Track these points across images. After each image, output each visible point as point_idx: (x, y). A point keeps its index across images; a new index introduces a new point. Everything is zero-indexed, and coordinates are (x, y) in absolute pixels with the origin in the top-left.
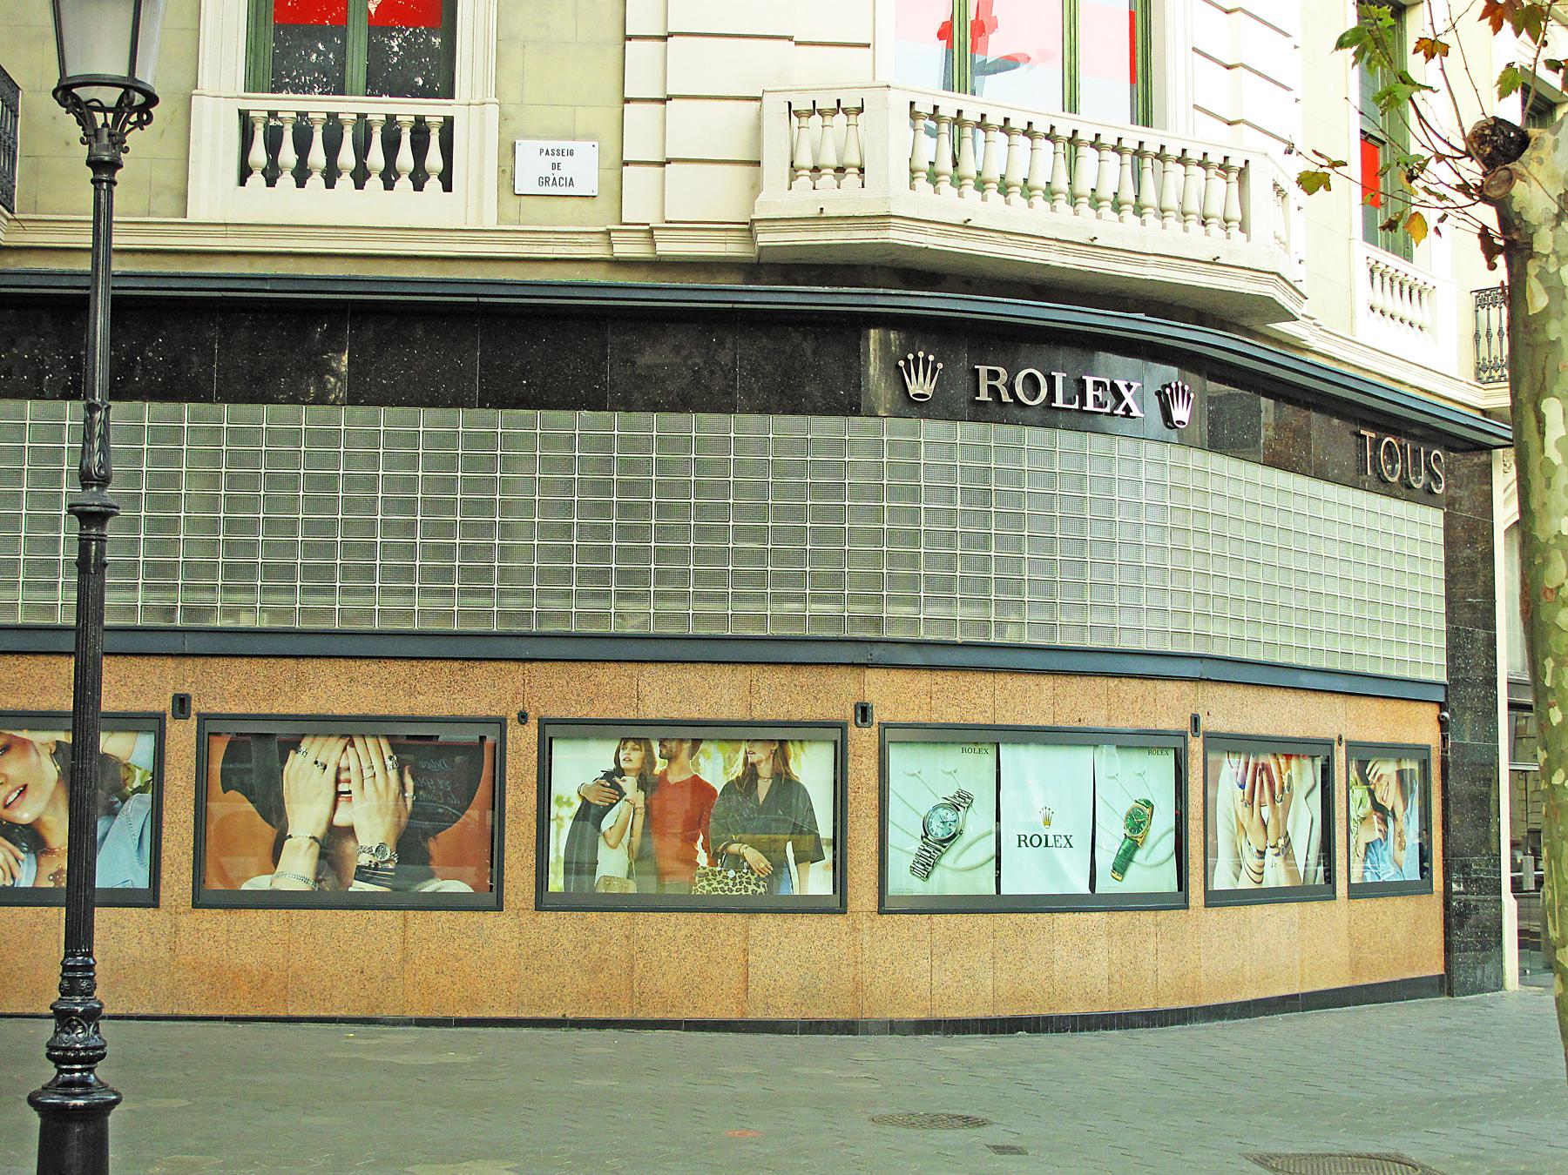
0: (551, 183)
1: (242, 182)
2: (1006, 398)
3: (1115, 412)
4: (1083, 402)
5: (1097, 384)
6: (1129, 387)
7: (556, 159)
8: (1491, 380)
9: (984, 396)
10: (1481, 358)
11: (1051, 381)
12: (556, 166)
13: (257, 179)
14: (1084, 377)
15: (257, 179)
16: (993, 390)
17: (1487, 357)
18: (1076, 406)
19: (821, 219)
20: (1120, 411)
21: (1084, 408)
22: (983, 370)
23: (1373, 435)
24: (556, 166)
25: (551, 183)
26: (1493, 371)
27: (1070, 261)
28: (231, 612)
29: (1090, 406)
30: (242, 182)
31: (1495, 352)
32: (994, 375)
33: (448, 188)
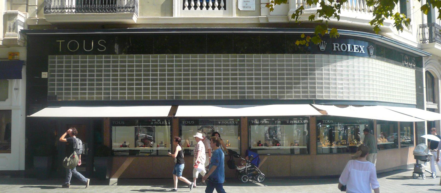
0: (246, 7)
1: (183, 9)
2: (339, 50)
3: (360, 52)
4: (354, 50)
5: (356, 47)
6: (362, 47)
7: (247, 3)
8: (58, 12)
9: (335, 49)
10: (55, 6)
11: (347, 46)
12: (246, 4)
13: (187, 8)
14: (354, 45)
15: (187, 8)
16: (337, 48)
17: (68, 5)
18: (352, 51)
19: (355, 19)
20: (360, 52)
21: (354, 52)
22: (335, 44)
23: (363, 52)
24: (246, 4)
25: (246, 7)
26: (55, 10)
27: (349, 22)
28: (288, 97)
29: (355, 51)
30: (183, 9)
31: (56, 4)
32: (337, 45)
33: (225, 9)
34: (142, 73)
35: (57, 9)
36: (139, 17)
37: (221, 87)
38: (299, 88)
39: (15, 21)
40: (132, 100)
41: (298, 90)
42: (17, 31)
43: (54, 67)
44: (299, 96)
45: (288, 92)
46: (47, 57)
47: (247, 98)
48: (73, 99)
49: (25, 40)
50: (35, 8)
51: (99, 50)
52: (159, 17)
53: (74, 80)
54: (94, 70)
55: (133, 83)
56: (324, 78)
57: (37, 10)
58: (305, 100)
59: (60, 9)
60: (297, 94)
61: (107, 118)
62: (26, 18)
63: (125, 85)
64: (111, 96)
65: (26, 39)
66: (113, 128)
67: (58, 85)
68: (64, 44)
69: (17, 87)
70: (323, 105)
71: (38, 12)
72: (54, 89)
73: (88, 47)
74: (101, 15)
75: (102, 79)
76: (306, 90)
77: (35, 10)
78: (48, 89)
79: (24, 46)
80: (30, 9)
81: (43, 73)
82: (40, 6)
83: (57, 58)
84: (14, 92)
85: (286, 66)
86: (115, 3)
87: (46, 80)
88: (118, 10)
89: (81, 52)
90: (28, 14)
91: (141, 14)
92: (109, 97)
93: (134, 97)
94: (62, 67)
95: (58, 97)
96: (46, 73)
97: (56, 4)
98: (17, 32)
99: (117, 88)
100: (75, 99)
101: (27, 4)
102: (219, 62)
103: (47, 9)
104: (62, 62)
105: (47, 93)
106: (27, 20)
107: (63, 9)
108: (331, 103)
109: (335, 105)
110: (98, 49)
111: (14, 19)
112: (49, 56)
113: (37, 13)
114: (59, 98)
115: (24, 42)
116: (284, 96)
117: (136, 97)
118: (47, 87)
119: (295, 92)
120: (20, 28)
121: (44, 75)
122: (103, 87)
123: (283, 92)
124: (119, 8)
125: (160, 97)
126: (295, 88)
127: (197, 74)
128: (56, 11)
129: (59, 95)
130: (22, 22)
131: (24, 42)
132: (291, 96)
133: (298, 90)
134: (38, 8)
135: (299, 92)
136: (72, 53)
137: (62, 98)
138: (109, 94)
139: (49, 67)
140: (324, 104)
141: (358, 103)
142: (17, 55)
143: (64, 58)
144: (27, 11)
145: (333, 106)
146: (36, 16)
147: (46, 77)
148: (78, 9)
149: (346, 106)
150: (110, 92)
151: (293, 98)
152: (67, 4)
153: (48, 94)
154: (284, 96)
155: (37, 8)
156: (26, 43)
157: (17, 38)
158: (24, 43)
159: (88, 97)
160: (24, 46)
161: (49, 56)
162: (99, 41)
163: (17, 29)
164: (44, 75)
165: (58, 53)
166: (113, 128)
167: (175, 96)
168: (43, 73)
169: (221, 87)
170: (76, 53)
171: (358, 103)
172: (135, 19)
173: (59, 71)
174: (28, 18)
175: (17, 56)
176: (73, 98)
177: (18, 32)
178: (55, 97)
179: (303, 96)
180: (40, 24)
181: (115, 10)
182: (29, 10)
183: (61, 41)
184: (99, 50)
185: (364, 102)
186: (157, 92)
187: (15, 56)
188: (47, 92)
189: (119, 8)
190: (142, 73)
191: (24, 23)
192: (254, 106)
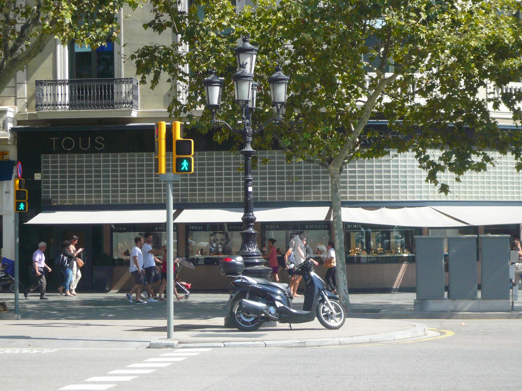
28: (306, 198)
31: (49, 100)
34: (127, 158)
35: (49, 105)
36: (140, 110)
37: (231, 188)
38: (319, 188)
39: (4, 118)
40: (125, 203)
41: (318, 190)
42: (7, 129)
43: (48, 167)
44: (319, 198)
45: (306, 193)
46: (40, 157)
47: (260, 200)
48: (69, 203)
49: (15, 137)
50: (24, 102)
51: (97, 148)
52: (162, 110)
53: (70, 182)
54: (92, 170)
55: (135, 185)
56: (401, 170)
57: (27, 103)
58: (325, 202)
59: (53, 105)
60: (316, 196)
61: (107, 224)
62: (15, 112)
63: (126, 187)
64: (110, 199)
65: (16, 136)
66: (115, 234)
67: (53, 187)
68: (58, 143)
69: (7, 191)
70: (347, 207)
71: (28, 105)
72: (48, 192)
73: (85, 145)
74: (97, 112)
75: (100, 180)
76: (345, 190)
77: (24, 103)
78: (42, 193)
79: (14, 144)
80: (19, 102)
81: (36, 174)
82: (30, 99)
83: (50, 158)
84: (5, 195)
85: (258, 177)
86: (113, 98)
87: (39, 182)
88: (115, 106)
89: (77, 151)
90: (17, 107)
91: (143, 106)
92: (109, 200)
93: (223, 198)
94: (56, 167)
95: (53, 201)
96: (40, 174)
97: (49, 100)
98: (6, 131)
99: (118, 190)
100: (72, 203)
101: (15, 97)
102: (229, 160)
103: (38, 105)
104: (56, 162)
105: (41, 197)
106: (16, 116)
107: (57, 105)
108: (357, 205)
109: (362, 207)
110: (96, 147)
111: (4, 116)
112: (42, 156)
113: (27, 107)
114: (54, 202)
115: (14, 139)
116: (301, 198)
117: (207, 199)
118: (40, 190)
119: (315, 193)
120: (10, 126)
121: (38, 176)
122: (102, 189)
123: (301, 193)
124: (116, 104)
125: (287, 198)
126: (314, 188)
127: (205, 168)
128: (49, 107)
129: (53, 198)
130: (11, 118)
131: (14, 139)
132: (310, 198)
133: (318, 190)
134: (27, 101)
135: (318, 193)
136: (67, 152)
137: (57, 202)
138: (117, 196)
139: (42, 167)
140: (347, 206)
141: (395, 205)
142: (6, 154)
143: (59, 157)
144: (16, 105)
145: (360, 209)
146: (26, 110)
147: (39, 178)
148: (72, 105)
149: (379, 207)
150: (109, 195)
151: (312, 200)
152: (60, 100)
153: (42, 198)
154: (301, 198)
155: (26, 100)
156: (16, 141)
157: (8, 137)
158: (14, 141)
159: (217, 199)
160: (14, 144)
161: (42, 156)
162: (96, 138)
163: (7, 127)
164: (38, 176)
165: (51, 152)
166: (115, 234)
167: (181, 199)
168: (36, 174)
169: (231, 188)
170: (73, 152)
171: (395, 205)
172: (134, 114)
173: (53, 172)
174: (17, 112)
175: (8, 156)
176: (70, 201)
177: (8, 130)
178: (50, 201)
179: (323, 198)
180: (31, 119)
181: (113, 106)
182: (18, 103)
183: (54, 139)
184: (97, 148)
185: (420, 203)
186: (161, 194)
187: (5, 156)
188: (41, 195)
189: (116, 104)
190: (127, 158)
191: (13, 118)
192: (266, 210)
